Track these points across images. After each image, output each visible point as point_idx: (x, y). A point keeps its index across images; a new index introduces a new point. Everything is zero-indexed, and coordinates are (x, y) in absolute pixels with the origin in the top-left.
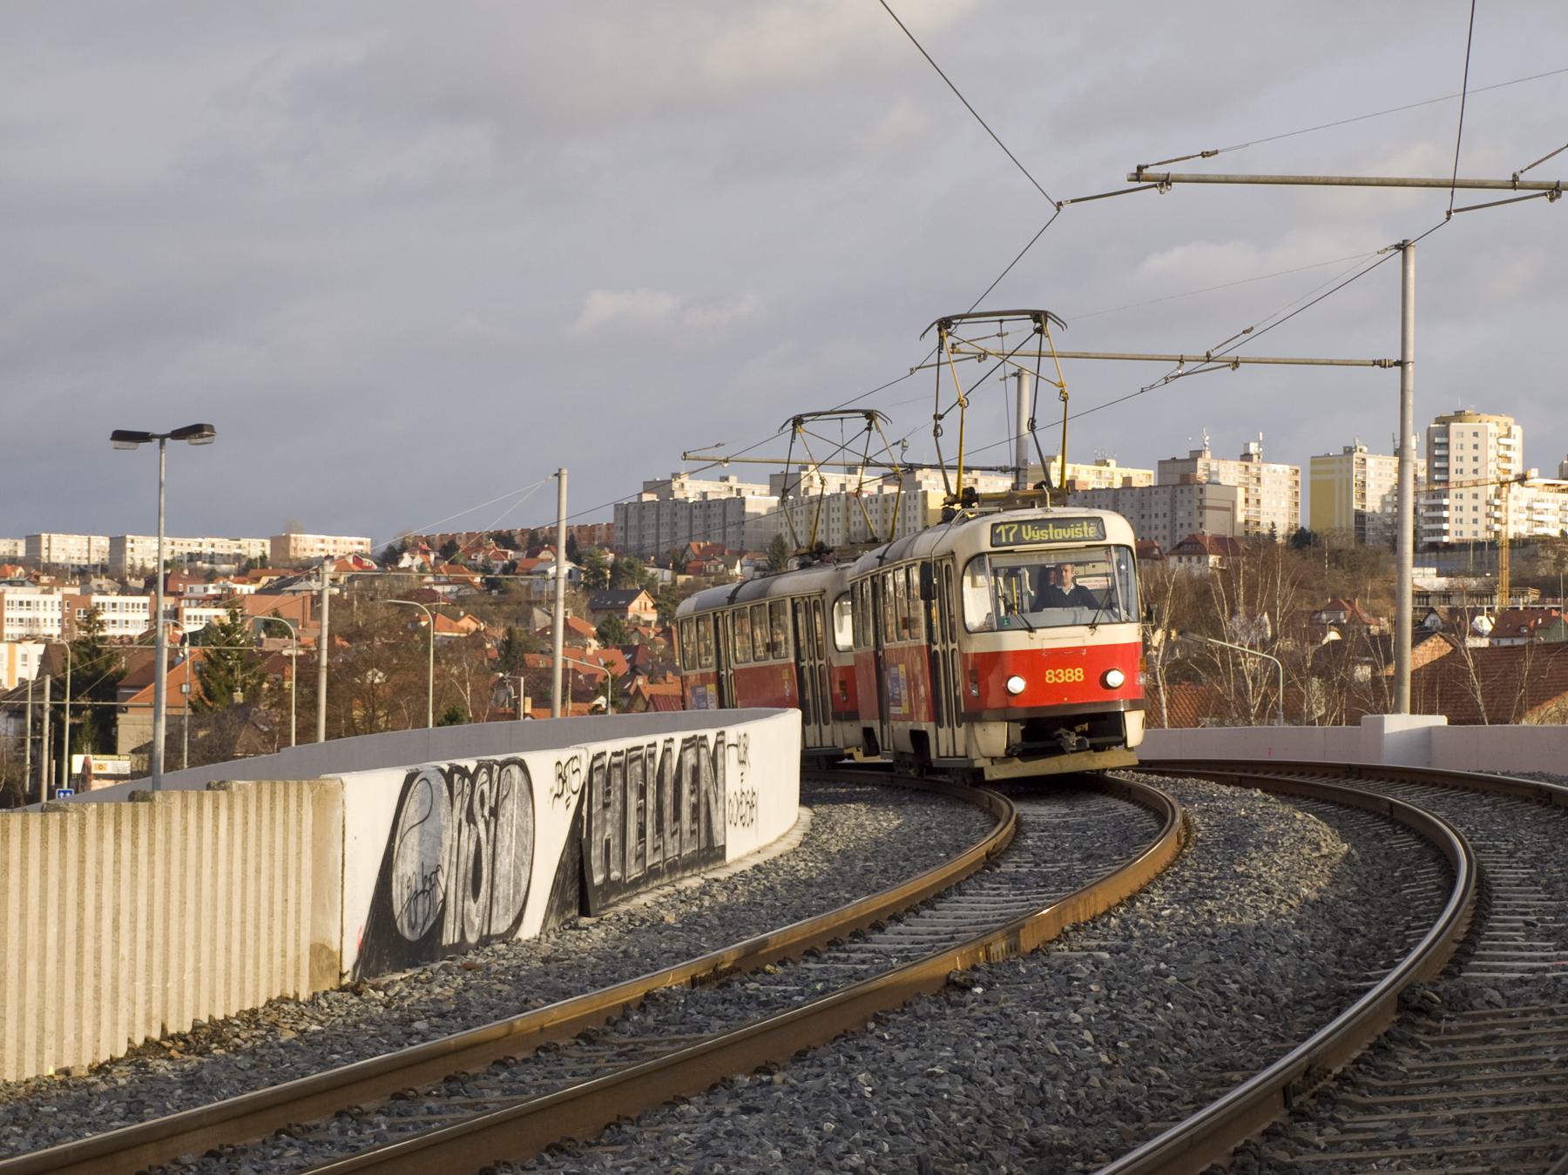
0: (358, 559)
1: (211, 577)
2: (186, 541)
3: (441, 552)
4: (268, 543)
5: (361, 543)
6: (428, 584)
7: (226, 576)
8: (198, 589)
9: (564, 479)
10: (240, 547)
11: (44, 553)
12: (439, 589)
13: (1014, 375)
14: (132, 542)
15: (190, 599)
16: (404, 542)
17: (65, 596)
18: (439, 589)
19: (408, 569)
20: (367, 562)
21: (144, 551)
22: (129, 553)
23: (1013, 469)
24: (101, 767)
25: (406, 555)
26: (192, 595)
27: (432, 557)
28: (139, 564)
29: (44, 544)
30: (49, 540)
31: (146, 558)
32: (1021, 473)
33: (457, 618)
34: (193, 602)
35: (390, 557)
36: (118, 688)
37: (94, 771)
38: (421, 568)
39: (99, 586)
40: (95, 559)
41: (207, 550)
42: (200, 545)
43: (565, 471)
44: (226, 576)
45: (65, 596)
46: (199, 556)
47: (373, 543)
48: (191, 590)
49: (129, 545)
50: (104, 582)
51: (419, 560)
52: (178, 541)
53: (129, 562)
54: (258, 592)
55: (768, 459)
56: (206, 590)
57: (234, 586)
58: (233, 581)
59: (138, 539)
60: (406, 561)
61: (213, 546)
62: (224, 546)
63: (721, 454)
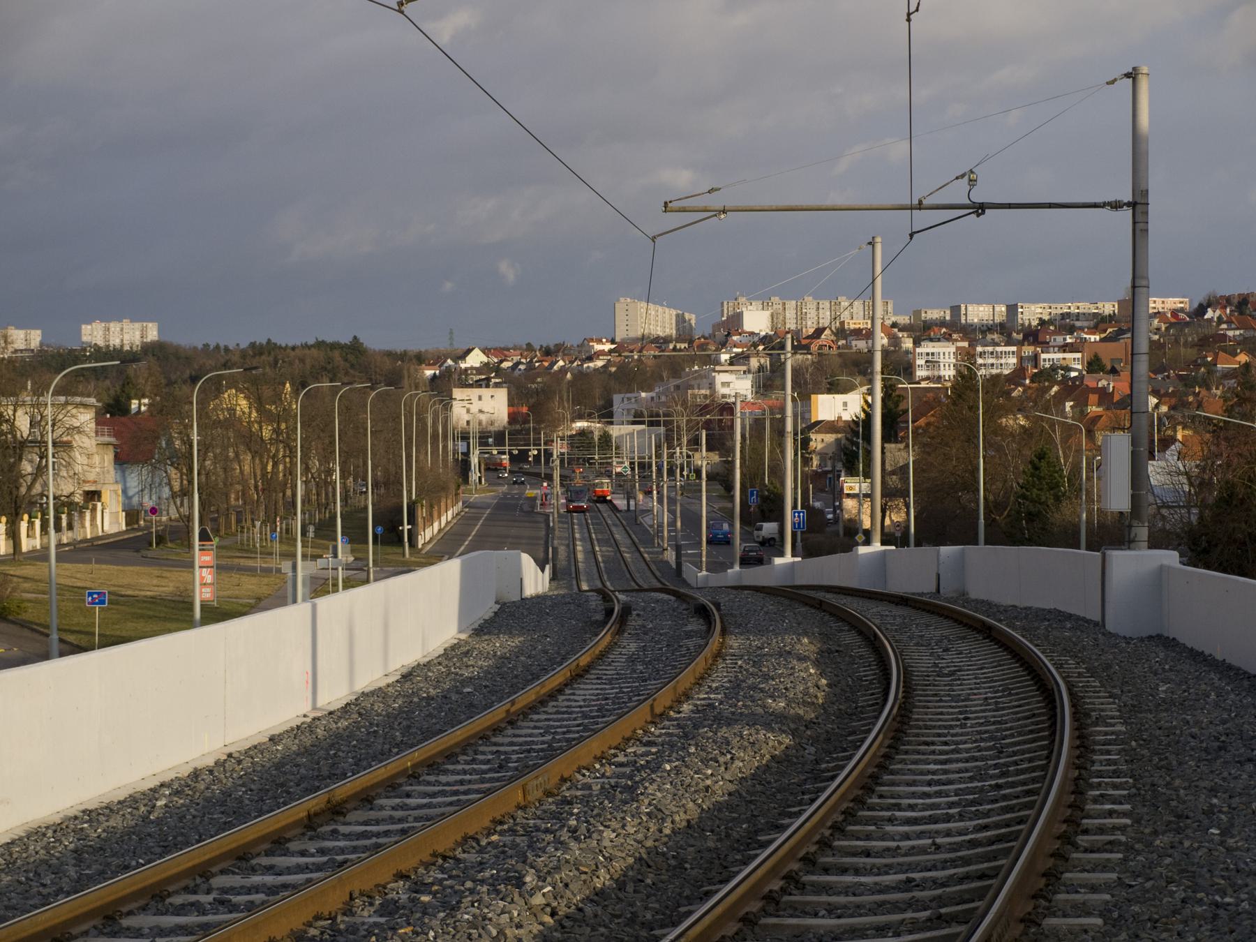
0: (1175, 313)
1: (1071, 330)
2: (1059, 306)
3: (1236, 307)
4: (948, 312)
5: (1181, 302)
6: (1222, 330)
7: (1081, 329)
8: (1059, 339)
9: (879, 248)
10: (1097, 308)
11: (963, 318)
12: (1230, 333)
13: (1128, 75)
14: (1155, 302)
15: (1054, 347)
16: (1209, 300)
17: (958, 348)
18: (1230, 333)
19: (1211, 320)
20: (1182, 315)
21: (1031, 313)
22: (1020, 316)
23: (1128, 204)
24: (851, 488)
25: (1209, 310)
26: (1055, 344)
27: (1228, 311)
28: (1027, 323)
29: (963, 311)
30: (966, 309)
31: (1032, 318)
32: (1138, 207)
33: (1235, 355)
34: (1056, 349)
35: (1201, 310)
36: (897, 423)
37: (846, 491)
38: (1220, 318)
39: (993, 339)
40: (998, 320)
41: (1074, 310)
42: (1070, 308)
43: (878, 239)
44: (1081, 329)
45: (958, 348)
46: (1068, 314)
47: (1191, 301)
48: (1055, 340)
49: (1020, 310)
50: (996, 336)
51: (1218, 312)
52: (1053, 306)
53: (1020, 321)
54: (1102, 340)
55: (781, 204)
56: (1065, 339)
57: (1087, 336)
58: (1087, 333)
59: (1025, 305)
60: (1209, 314)
61: (1078, 308)
62: (1085, 307)
63: (716, 201)
